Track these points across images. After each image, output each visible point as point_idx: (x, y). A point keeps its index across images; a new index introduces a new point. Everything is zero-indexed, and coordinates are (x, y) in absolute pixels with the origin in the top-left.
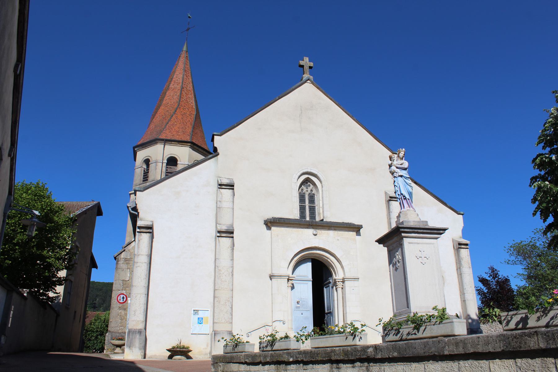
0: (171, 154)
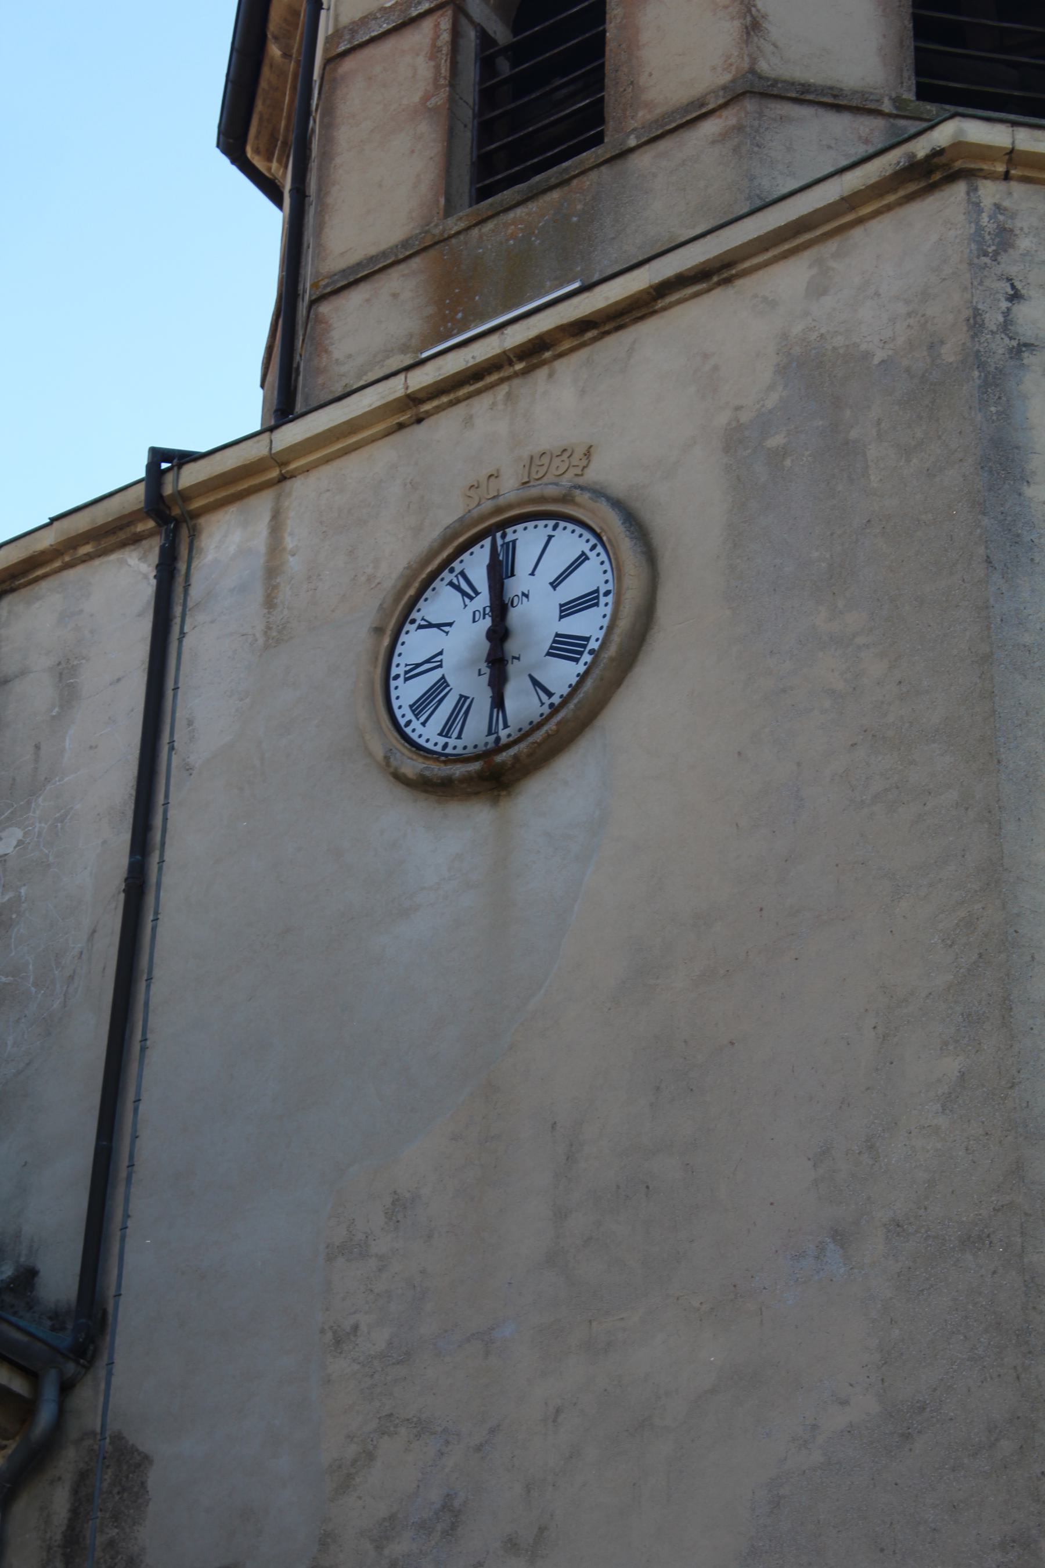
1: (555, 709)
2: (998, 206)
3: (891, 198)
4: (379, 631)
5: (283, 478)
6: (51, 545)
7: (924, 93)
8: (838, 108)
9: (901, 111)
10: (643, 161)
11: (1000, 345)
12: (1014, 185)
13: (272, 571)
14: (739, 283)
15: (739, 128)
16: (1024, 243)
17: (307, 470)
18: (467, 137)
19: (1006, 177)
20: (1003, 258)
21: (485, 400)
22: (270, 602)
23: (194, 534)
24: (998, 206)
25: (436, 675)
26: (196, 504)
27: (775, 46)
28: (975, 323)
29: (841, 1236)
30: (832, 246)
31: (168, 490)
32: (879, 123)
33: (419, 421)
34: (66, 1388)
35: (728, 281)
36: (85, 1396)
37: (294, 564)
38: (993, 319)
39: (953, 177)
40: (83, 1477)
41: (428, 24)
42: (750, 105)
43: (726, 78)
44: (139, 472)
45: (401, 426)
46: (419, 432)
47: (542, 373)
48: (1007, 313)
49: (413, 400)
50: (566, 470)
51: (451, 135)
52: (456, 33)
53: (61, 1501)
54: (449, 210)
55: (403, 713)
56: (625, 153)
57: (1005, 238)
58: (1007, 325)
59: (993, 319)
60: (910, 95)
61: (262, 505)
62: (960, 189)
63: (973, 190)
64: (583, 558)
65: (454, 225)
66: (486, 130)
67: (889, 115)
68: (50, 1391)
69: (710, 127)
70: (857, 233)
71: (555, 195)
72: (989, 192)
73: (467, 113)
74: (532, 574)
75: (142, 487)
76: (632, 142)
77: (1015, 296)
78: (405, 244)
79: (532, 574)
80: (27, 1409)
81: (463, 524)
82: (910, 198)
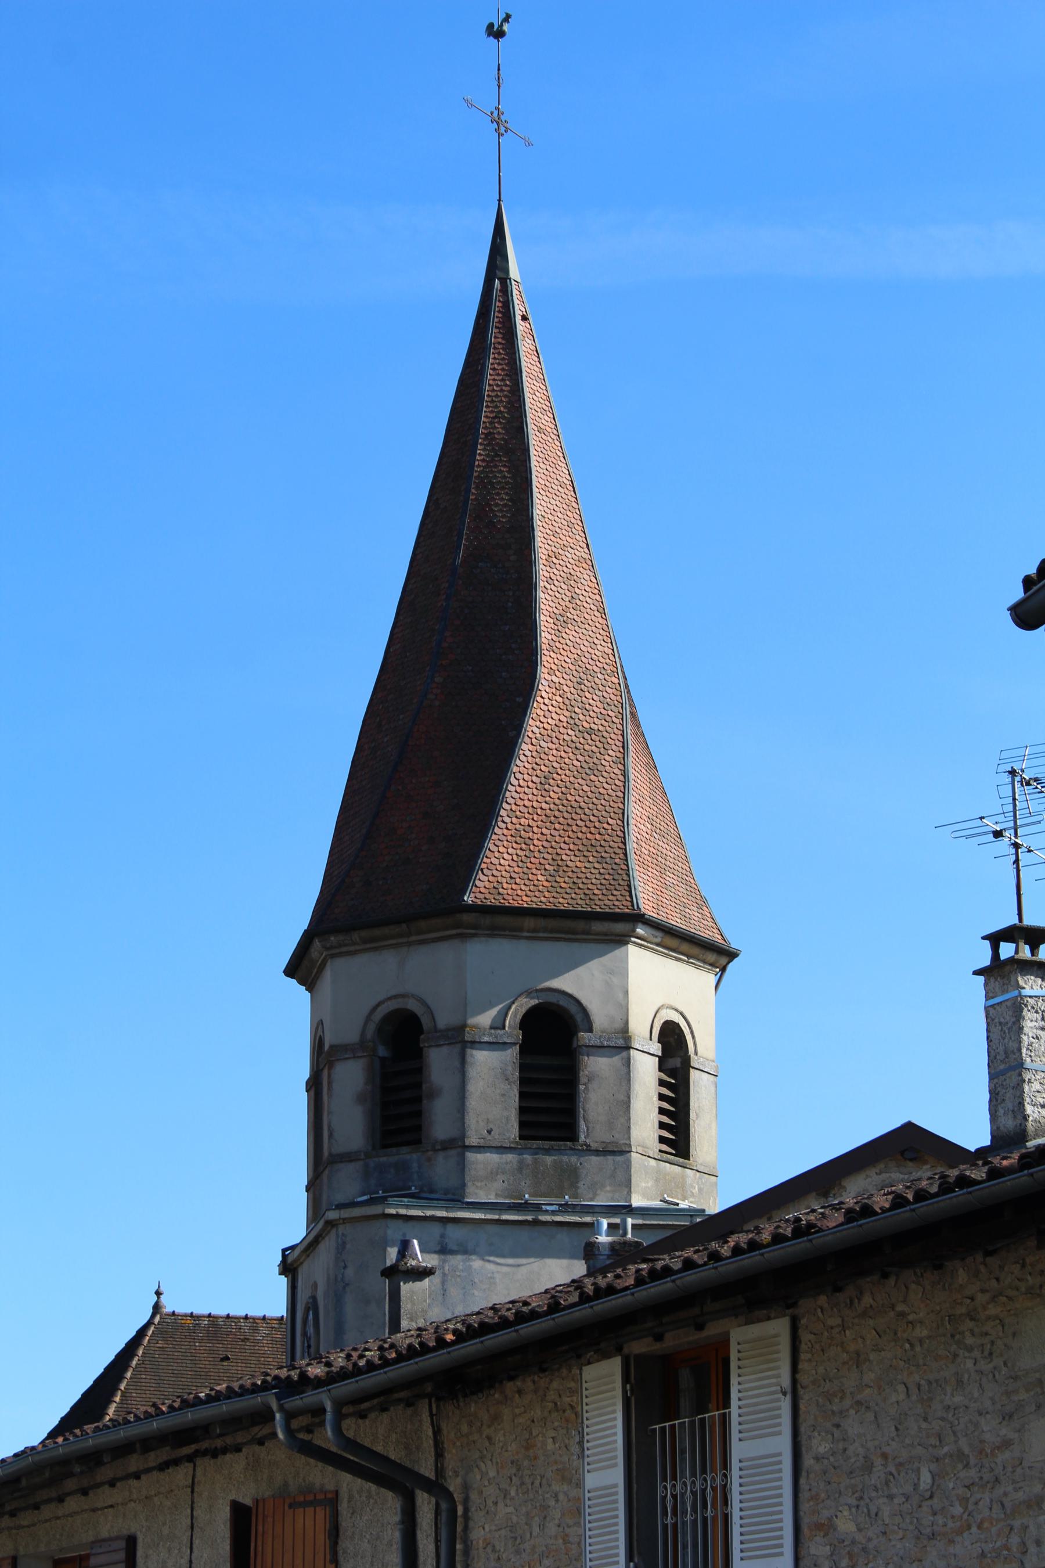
0: (395, 997)
8: (351, 1161)
16: (348, 1246)
24: (343, 1234)
26: (295, 1266)
27: (336, 1141)
32: (361, 1163)
48: (343, 1274)
57: (344, 1243)
67: (363, 1159)
72: (341, 1229)
74: (716, 1076)
77: (345, 1267)
79: (716, 1076)
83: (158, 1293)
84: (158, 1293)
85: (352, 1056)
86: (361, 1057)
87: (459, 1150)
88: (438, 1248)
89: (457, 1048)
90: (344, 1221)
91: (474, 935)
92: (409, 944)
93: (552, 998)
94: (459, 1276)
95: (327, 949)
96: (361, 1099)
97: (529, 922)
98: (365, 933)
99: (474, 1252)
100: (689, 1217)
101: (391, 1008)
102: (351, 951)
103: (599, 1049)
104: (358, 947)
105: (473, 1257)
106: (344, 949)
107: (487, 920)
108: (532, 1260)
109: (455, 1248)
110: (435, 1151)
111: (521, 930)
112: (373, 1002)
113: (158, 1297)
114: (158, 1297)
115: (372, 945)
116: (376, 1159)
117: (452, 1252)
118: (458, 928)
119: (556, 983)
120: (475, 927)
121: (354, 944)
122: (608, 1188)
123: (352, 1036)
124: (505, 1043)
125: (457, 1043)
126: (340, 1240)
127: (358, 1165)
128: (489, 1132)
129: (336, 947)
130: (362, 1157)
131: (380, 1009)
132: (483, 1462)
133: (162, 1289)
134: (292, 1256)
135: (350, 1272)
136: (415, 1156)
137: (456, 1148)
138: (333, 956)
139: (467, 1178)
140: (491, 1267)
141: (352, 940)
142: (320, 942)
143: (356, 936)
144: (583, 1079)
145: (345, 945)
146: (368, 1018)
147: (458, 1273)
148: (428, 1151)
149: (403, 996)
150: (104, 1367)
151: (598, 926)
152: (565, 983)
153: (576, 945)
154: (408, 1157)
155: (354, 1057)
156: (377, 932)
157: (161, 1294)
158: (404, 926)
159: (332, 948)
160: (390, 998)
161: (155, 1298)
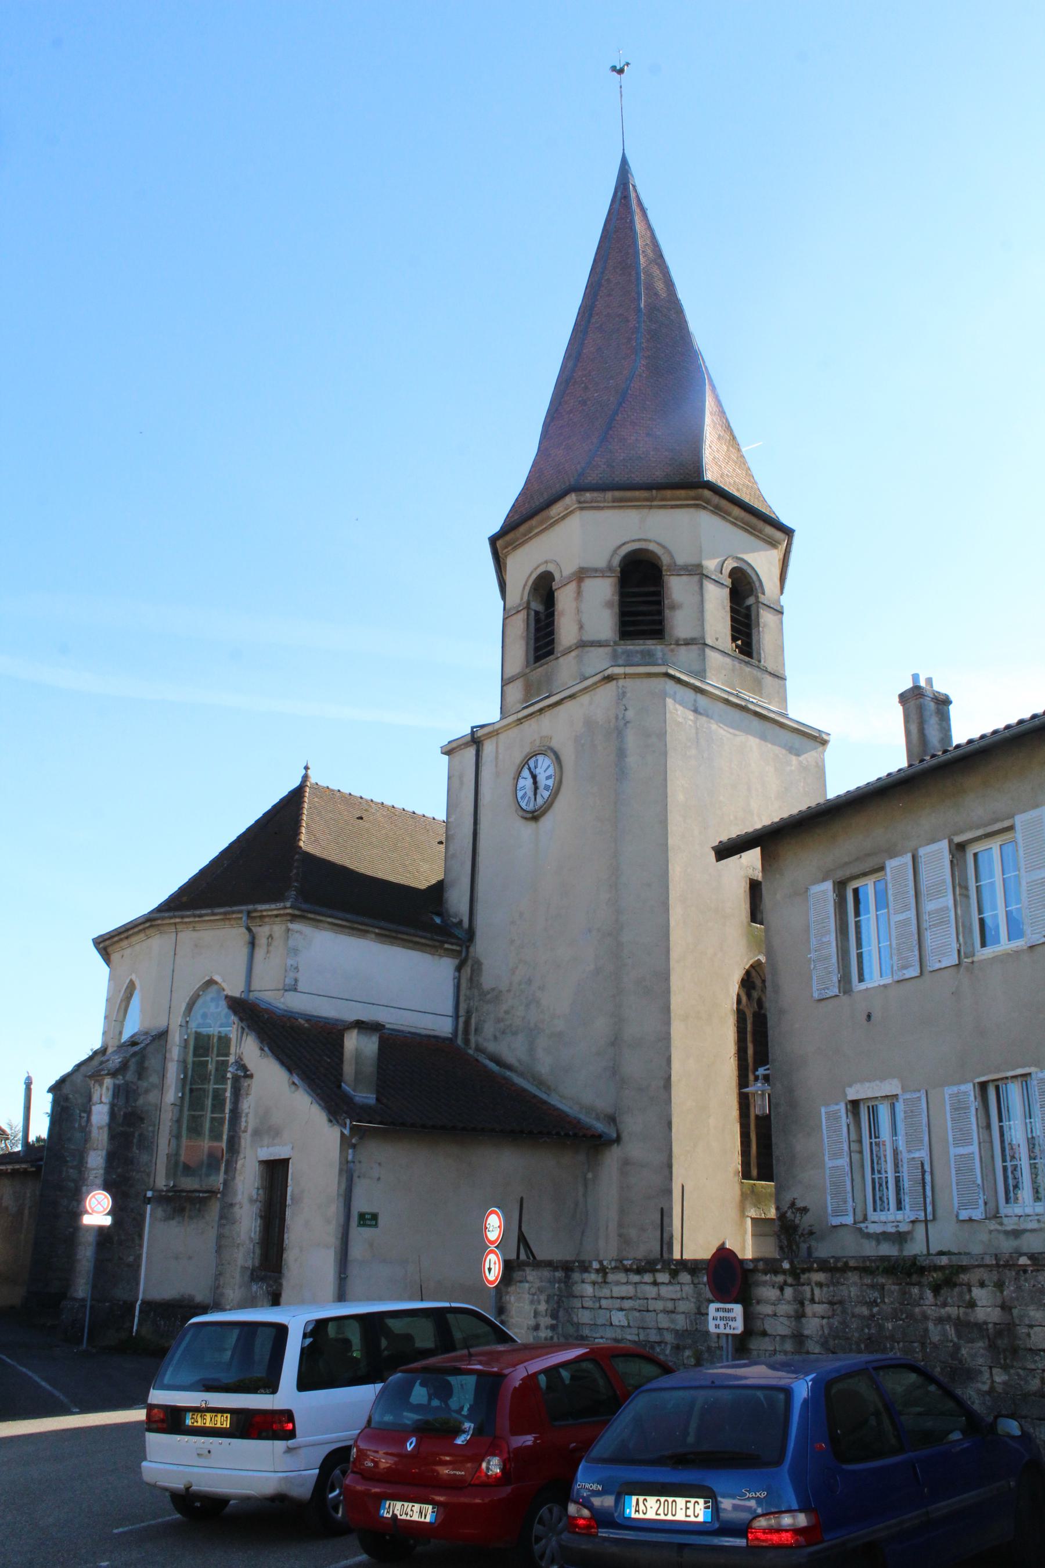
0: (639, 540)
1: (545, 802)
2: (623, 686)
3: (602, 683)
4: (514, 779)
5: (498, 734)
6: (87, 1163)
7: (621, 639)
9: (616, 644)
10: (561, 660)
11: (622, 723)
12: (627, 680)
13: (497, 758)
14: (578, 698)
15: (577, 656)
16: (628, 695)
17: (502, 732)
18: (532, 642)
19: (625, 678)
20: (624, 699)
21: (533, 720)
22: (496, 766)
23: (482, 745)
24: (623, 686)
25: (525, 791)
26: (482, 739)
28: (617, 718)
29: (590, 931)
30: (592, 693)
31: (476, 736)
32: (609, 648)
33: (521, 723)
34: (468, 948)
35: (575, 698)
36: (471, 949)
37: (501, 757)
38: (621, 716)
39: (614, 679)
40: (472, 966)
41: (522, 612)
42: (580, 649)
43: (575, 641)
44: (469, 731)
45: (518, 725)
46: (521, 725)
47: (543, 715)
48: (624, 714)
49: (519, 720)
50: (305, 993)
51: (527, 644)
52: (528, 615)
53: (469, 970)
54: (527, 667)
55: (519, 800)
56: (557, 658)
57: (624, 693)
58: (623, 718)
59: (621, 716)
60: (618, 639)
61: (494, 739)
62: (615, 682)
63: (617, 682)
64: (549, 766)
65: (528, 671)
66: (537, 640)
68: (464, 950)
69: (573, 654)
70: (597, 690)
71: (545, 666)
72: (621, 682)
73: (532, 636)
75: (470, 735)
76: (559, 655)
77: (626, 710)
78: (519, 674)
80: (460, 952)
81: (529, 754)
82: (606, 683)
83: (306, 768)
84: (306, 768)
85: (601, 575)
86: (609, 577)
87: (700, 646)
88: (693, 708)
89: (696, 578)
90: (626, 676)
91: (705, 508)
92: (651, 507)
93: (745, 567)
94: (705, 732)
95: (580, 502)
96: (609, 604)
97: (737, 511)
98: (618, 494)
99: (712, 718)
100: (173, 927)
101: (634, 548)
102: (599, 507)
103: (768, 608)
104: (606, 504)
105: (712, 721)
106: (595, 505)
107: (716, 499)
108: (741, 733)
109: (702, 711)
110: (678, 644)
111: (729, 514)
112: (619, 542)
113: (306, 771)
114: (306, 771)
115: (620, 504)
116: (624, 647)
117: (700, 714)
118: (697, 500)
119: (746, 557)
120: (708, 502)
121: (605, 501)
122: (776, 699)
123: (601, 562)
124: (722, 584)
125: (695, 574)
126: (620, 690)
127: (608, 649)
128: (717, 639)
129: (587, 502)
130: (612, 644)
131: (624, 547)
132: (253, 991)
133: (309, 765)
134: (480, 733)
135: (630, 714)
136: (659, 647)
137: (696, 644)
138: (582, 509)
139: (707, 667)
140: (721, 731)
141: (604, 498)
142: (576, 496)
143: (609, 495)
144: (761, 625)
145: (598, 502)
146: (615, 551)
147: (704, 730)
148: (671, 644)
149: (645, 540)
150: (263, 813)
151: (769, 530)
152: (750, 558)
153: (752, 538)
154: (653, 647)
155: (603, 577)
156: (629, 494)
157: (309, 769)
158: (654, 492)
159: (585, 502)
160: (634, 541)
161: (304, 772)
